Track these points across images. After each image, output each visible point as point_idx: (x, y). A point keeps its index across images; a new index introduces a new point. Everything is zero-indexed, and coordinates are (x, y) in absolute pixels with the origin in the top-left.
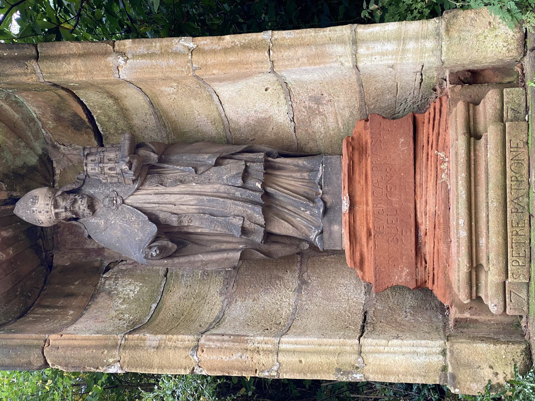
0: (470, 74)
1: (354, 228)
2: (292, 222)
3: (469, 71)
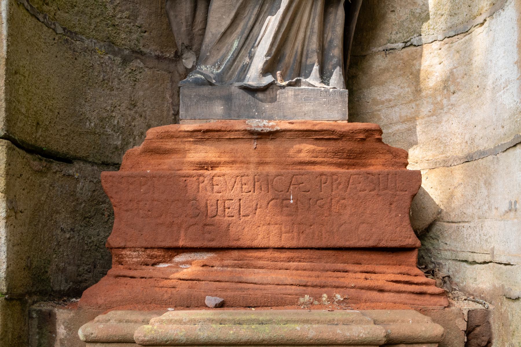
1: (219, 139)
2: (232, 33)
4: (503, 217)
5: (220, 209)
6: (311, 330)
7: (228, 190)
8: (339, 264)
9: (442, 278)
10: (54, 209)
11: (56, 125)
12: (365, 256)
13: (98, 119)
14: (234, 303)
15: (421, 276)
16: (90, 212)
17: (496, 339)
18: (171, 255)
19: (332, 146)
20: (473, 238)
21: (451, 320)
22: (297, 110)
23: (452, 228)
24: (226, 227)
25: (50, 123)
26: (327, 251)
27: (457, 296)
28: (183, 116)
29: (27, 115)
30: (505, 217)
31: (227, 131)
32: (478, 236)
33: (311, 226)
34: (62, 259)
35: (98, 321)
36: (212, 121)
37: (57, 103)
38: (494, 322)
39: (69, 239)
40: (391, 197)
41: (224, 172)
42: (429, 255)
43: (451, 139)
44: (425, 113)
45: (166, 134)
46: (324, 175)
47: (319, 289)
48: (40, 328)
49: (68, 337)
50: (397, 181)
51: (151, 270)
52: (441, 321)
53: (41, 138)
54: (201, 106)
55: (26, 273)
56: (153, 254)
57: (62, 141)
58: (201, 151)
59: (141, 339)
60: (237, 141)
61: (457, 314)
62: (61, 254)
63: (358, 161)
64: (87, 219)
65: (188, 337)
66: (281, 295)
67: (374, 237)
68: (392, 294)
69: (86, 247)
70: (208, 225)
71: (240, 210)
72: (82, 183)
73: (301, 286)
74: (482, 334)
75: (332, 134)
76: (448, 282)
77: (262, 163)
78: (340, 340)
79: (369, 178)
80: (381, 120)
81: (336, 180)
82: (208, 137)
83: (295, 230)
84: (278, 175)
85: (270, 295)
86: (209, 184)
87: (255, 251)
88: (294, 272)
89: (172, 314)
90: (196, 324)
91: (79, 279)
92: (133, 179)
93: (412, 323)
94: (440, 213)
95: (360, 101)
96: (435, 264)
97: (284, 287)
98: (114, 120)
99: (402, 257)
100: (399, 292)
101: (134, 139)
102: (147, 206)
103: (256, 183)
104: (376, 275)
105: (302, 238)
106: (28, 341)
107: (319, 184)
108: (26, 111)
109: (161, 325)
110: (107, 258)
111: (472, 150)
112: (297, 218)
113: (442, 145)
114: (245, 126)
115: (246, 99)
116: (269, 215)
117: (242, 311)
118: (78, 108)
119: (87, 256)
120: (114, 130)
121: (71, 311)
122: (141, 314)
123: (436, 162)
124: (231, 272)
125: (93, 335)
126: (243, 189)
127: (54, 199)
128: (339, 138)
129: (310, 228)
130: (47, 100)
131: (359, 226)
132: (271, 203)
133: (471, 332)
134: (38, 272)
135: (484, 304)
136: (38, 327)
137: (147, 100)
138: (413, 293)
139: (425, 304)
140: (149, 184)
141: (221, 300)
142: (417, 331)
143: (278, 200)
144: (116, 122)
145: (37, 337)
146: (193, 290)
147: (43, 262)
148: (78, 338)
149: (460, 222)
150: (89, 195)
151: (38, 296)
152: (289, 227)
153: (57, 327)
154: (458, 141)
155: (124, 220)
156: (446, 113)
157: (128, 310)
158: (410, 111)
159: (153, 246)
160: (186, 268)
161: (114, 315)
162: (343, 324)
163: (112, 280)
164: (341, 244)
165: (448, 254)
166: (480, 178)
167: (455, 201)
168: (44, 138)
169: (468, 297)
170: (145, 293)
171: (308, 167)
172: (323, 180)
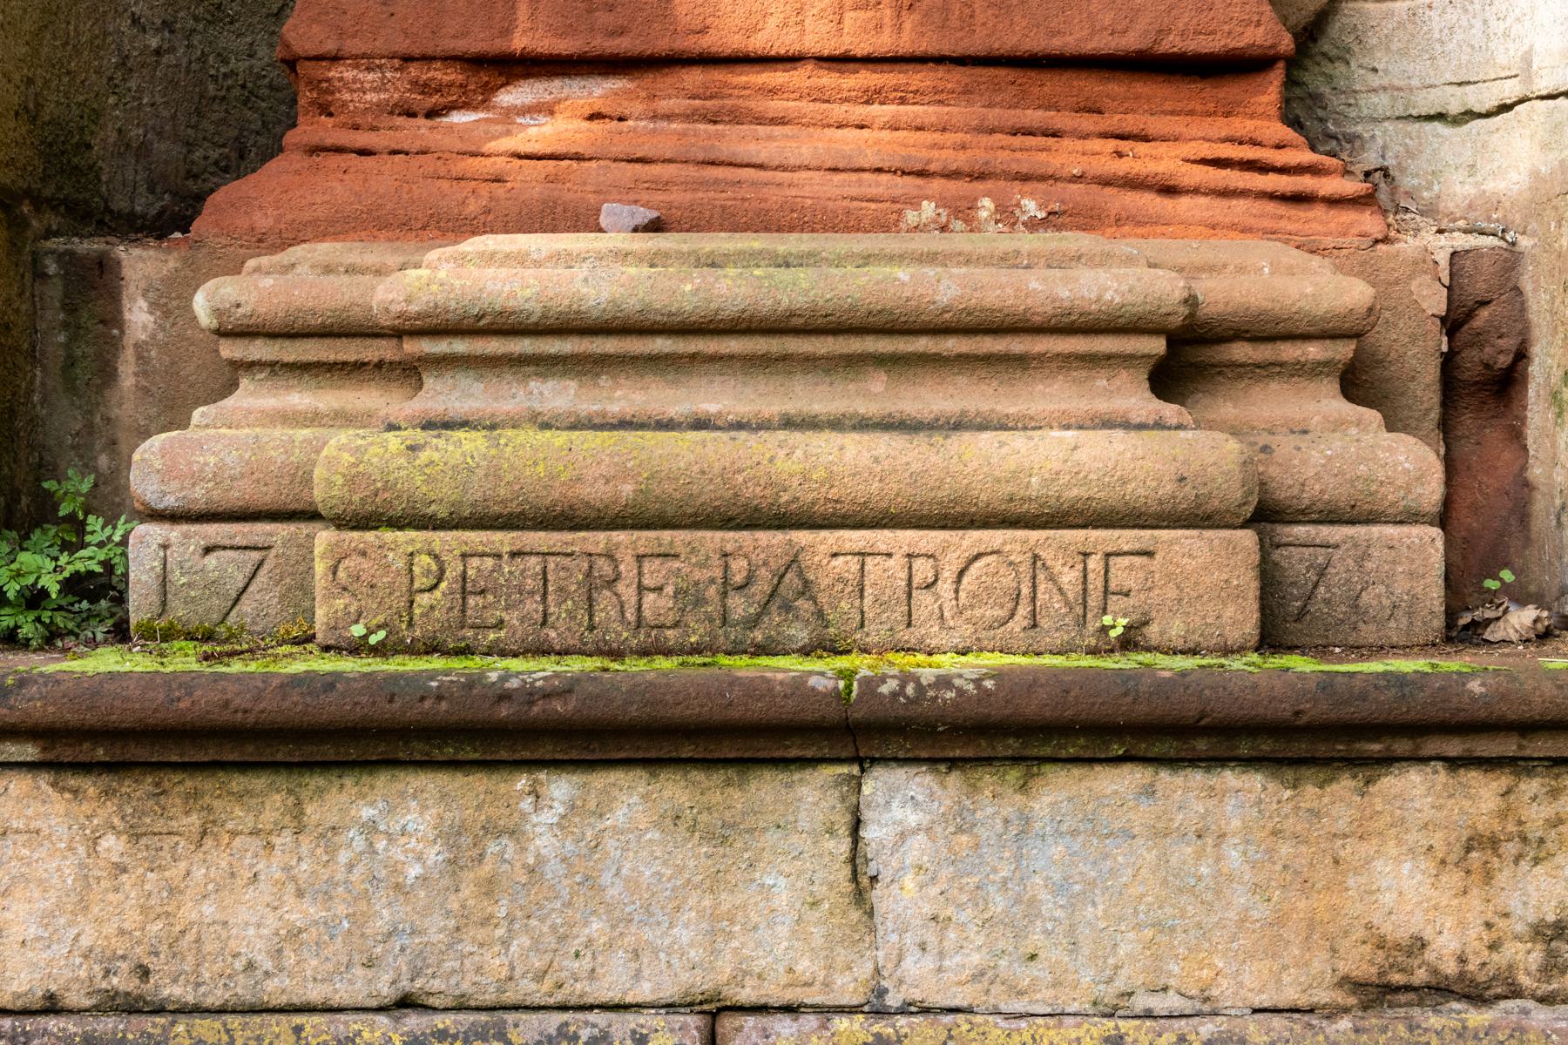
0: (1504, 361)
3: (1521, 355)
6: (945, 282)
8: (1029, 112)
15: (1297, 147)
21: (1397, 282)
23: (1393, 15)
34: (135, 114)
35: (257, 270)
38: (1535, 290)
39: (158, 52)
42: (1320, 113)
48: (70, 308)
49: (160, 336)
51: (422, 131)
55: (24, 130)
59: (396, 308)
61: (1415, 263)
65: (549, 304)
66: (846, 203)
67: (1141, 24)
68: (1202, 201)
73: (909, 174)
74: (1497, 328)
78: (1038, 314)
85: (809, 202)
87: (757, 68)
93: (1272, 273)
97: (854, 177)
99: (1231, 90)
100: (1226, 193)
104: (1152, 144)
105: (908, 26)
106: (34, 351)
119: (215, 117)
122: (395, 251)
124: (684, 134)
125: (240, 310)
133: (1462, 324)
136: (64, 307)
138: (1272, 196)
139: (1310, 232)
141: (655, 214)
145: (62, 338)
146: (560, 186)
147: (75, 111)
151: (63, 216)
153: (126, 303)
159: (430, 52)
162: (1049, 267)
165: (1381, 103)
170: (406, 196)
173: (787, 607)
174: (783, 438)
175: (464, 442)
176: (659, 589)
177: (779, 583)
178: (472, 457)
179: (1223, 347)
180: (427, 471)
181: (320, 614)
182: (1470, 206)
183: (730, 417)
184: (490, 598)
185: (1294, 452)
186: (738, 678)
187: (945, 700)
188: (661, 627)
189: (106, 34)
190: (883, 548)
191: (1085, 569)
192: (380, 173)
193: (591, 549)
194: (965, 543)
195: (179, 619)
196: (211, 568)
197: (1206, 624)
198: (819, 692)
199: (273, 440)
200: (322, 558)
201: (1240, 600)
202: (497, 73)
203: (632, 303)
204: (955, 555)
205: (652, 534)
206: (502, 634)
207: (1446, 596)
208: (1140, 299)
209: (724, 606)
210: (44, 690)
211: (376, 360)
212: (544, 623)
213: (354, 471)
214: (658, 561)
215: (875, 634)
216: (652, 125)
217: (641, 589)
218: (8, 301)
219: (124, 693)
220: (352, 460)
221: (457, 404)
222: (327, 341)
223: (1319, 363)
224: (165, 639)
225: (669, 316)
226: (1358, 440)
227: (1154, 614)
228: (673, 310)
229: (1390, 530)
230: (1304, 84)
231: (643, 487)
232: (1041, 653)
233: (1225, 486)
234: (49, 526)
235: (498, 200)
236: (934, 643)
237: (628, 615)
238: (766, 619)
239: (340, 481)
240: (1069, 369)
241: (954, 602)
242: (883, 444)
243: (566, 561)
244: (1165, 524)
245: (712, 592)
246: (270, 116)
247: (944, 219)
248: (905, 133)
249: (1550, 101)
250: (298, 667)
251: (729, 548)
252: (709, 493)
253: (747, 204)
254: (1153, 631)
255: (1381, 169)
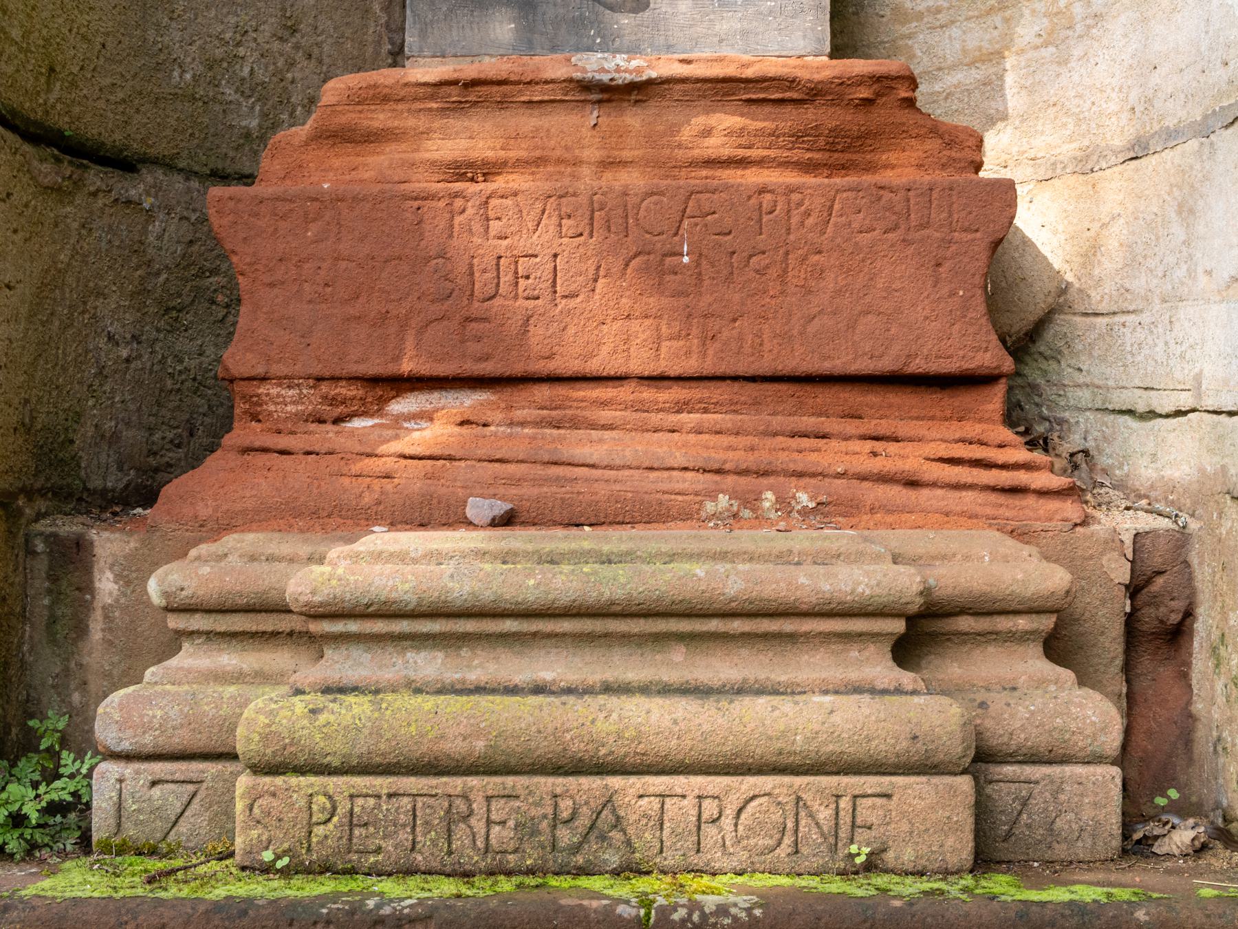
0: (1175, 618)
1: (503, 104)
3: (1189, 614)
4: (1224, 294)
5: (506, 279)
6: (732, 577)
7: (525, 232)
8: (805, 418)
9: (1068, 456)
10: (91, 284)
11: (96, 74)
12: (872, 398)
13: (201, 63)
14: (538, 515)
15: (1015, 446)
16: (180, 295)
17: (1207, 605)
18: (381, 396)
19: (789, 119)
20: (1148, 352)
21: (1091, 557)
22: (700, 29)
23: (1095, 328)
24: (520, 323)
25: (81, 69)
26: (776, 385)
27: (1107, 500)
28: (414, 48)
29: (25, 45)
30: (1231, 292)
31: (525, 84)
32: (1160, 348)
33: (735, 320)
35: (198, 558)
36: (487, 59)
37: (100, 19)
38: (1201, 564)
39: (128, 360)
40: (939, 246)
41: (516, 186)
42: (1037, 399)
43: (1093, 103)
44: (1027, 39)
45: (371, 92)
46: (769, 192)
47: (753, 480)
48: (54, 578)
49: (123, 601)
50: (955, 206)
51: (331, 435)
52: (1064, 559)
53: (59, 106)
54: (458, 22)
55: (20, 441)
56: (337, 395)
57: (112, 115)
58: (457, 133)
59: (303, 599)
60: (549, 108)
61: (1106, 542)
62: (109, 399)
63: (854, 157)
64: (172, 312)
65: (422, 596)
66: (659, 496)
67: (895, 349)
68: (939, 492)
69: (169, 383)
70: (476, 320)
71: (554, 282)
72: (162, 222)
73: (709, 471)
74: (1170, 593)
75: (790, 88)
76: (1084, 466)
77: (612, 163)
79: (884, 199)
80: (916, 61)
81: (800, 204)
82: (475, 99)
83: (695, 331)
84: (652, 194)
86: (478, 217)
87: (592, 385)
88: (692, 438)
89: (382, 539)
90: (441, 564)
91: (153, 461)
92: (288, 206)
93: (991, 561)
94: (1063, 290)
95: (862, 14)
96: (1050, 421)
97: (666, 474)
98: (242, 67)
99: (965, 399)
100: (958, 487)
101: (292, 115)
102: (322, 272)
103: (597, 214)
104: (901, 444)
105: (711, 352)
106: (25, 612)
107: (755, 216)
108: (23, 37)
109: (353, 566)
110: (221, 411)
111: (1148, 128)
112: (699, 301)
113: (1070, 120)
114: (571, 69)
115: (573, 5)
116: (628, 293)
117: (560, 532)
118: (151, 34)
119: (171, 405)
120: (243, 92)
121: (132, 535)
122: (306, 541)
123: (1054, 164)
124: (534, 438)
125: (183, 593)
126: (564, 230)
127: (91, 259)
128: (807, 97)
129: (732, 325)
130: (76, 12)
131: (856, 320)
132: (633, 263)
133: (1143, 588)
134: (51, 440)
135: (1177, 516)
136: (49, 577)
137: (324, 17)
138: (994, 489)
140: (327, 218)
141: (507, 506)
142: (1004, 583)
143: (652, 257)
144: (246, 70)
145: (46, 602)
146: (436, 482)
147: (62, 416)
148: (148, 603)
149: (1114, 313)
150: (178, 252)
151: (50, 500)
152: (678, 323)
153: (97, 575)
154: (1113, 107)
155: (264, 310)
156: (1080, 37)
157: (273, 530)
158: (988, 37)
159: (337, 374)
160: (418, 430)
161: (237, 542)
162: (815, 563)
163: (234, 460)
164: (810, 366)
165: (1084, 396)
166: (1166, 197)
167: (1103, 259)
168: (68, 106)
169: (1134, 503)
170: (315, 491)
171: (728, 172)
172: (764, 206)
173: (603, 837)
174: (602, 702)
175: (354, 706)
176: (503, 823)
177: (597, 818)
178: (360, 719)
179: (951, 620)
180: (325, 730)
181: (239, 841)
182: (1152, 486)
183: (562, 684)
184: (371, 829)
185: (1005, 707)
186: (562, 906)
187: (723, 926)
188: (505, 852)
189: (87, 352)
190: (679, 791)
191: (837, 807)
192: (296, 471)
193: (451, 791)
194: (744, 787)
195: (130, 837)
196: (156, 797)
197: (932, 852)
198: (625, 919)
199: (207, 696)
200: (241, 798)
201: (959, 833)
202: (389, 389)
203: (487, 594)
204: (735, 797)
205: (498, 779)
206: (380, 857)
207: (1124, 804)
208: (885, 592)
209: (554, 836)
210: (23, 915)
211: (288, 630)
212: (413, 849)
213: (268, 730)
214: (503, 801)
215: (671, 859)
216: (509, 430)
217: (489, 822)
218: (6, 578)
219: (84, 918)
220: (267, 721)
221: (350, 673)
222: (251, 615)
223: (1027, 632)
224: (118, 854)
225: (516, 604)
226: (1055, 697)
227: (890, 843)
228: (520, 600)
229: (1080, 770)
230: (1024, 375)
231: (492, 743)
232: (802, 874)
233: (949, 743)
234: (32, 755)
235: (387, 494)
236: (717, 865)
237: (478, 843)
238: (586, 846)
239: (257, 738)
240: (829, 643)
241: (734, 834)
242: (683, 708)
243: (431, 801)
244: (901, 771)
245: (545, 824)
246: (215, 401)
247: (735, 508)
248: (706, 437)
249: (1215, 416)
250: (220, 892)
251: (558, 791)
252: (544, 748)
253: (581, 497)
254: (890, 856)
255: (1082, 451)
